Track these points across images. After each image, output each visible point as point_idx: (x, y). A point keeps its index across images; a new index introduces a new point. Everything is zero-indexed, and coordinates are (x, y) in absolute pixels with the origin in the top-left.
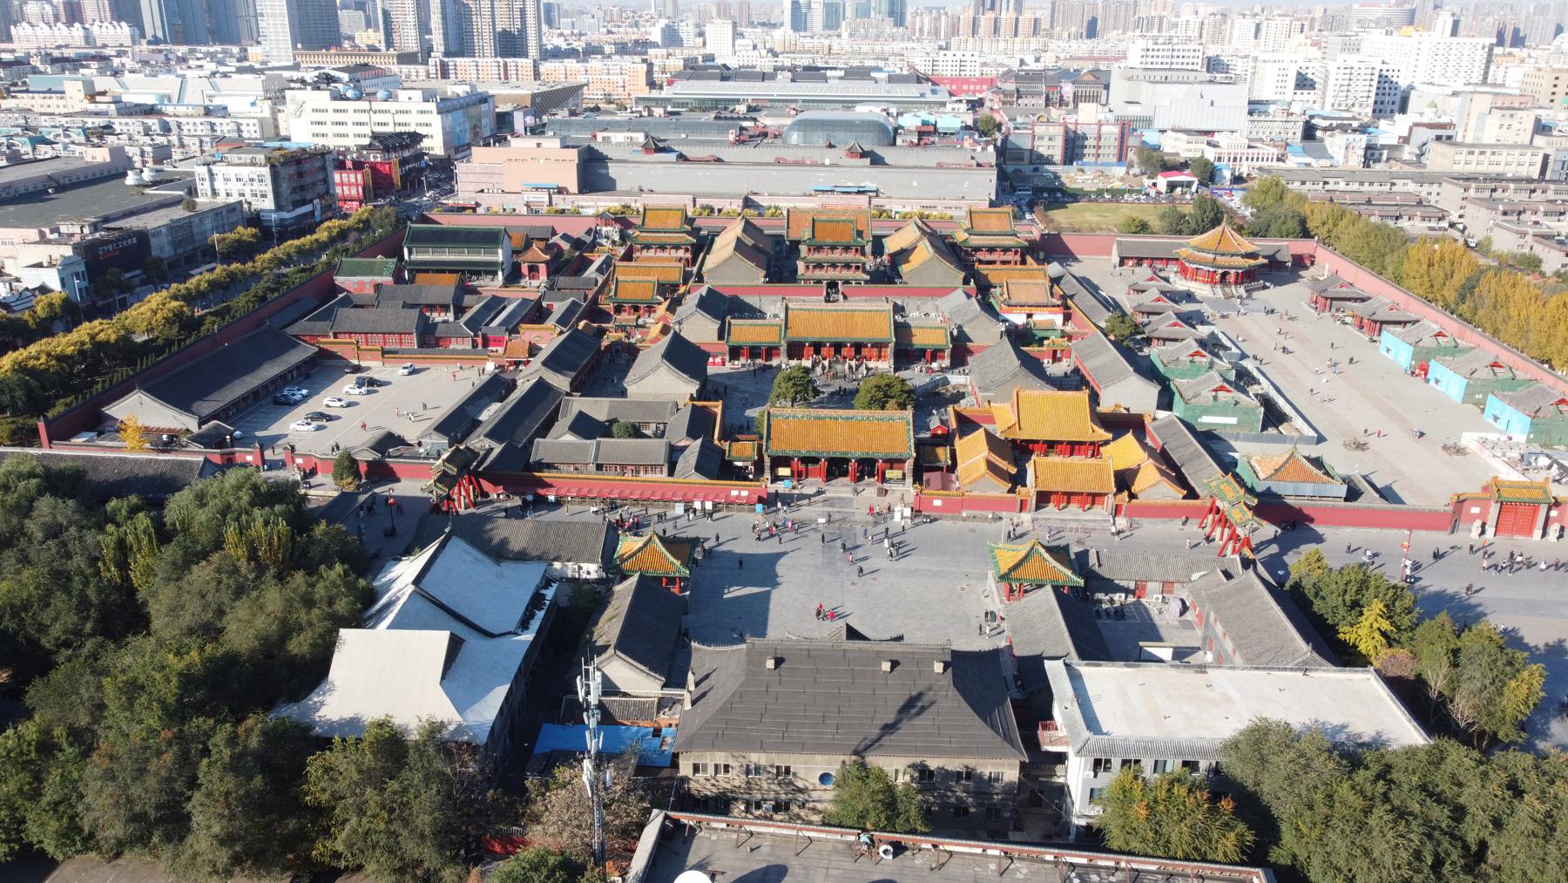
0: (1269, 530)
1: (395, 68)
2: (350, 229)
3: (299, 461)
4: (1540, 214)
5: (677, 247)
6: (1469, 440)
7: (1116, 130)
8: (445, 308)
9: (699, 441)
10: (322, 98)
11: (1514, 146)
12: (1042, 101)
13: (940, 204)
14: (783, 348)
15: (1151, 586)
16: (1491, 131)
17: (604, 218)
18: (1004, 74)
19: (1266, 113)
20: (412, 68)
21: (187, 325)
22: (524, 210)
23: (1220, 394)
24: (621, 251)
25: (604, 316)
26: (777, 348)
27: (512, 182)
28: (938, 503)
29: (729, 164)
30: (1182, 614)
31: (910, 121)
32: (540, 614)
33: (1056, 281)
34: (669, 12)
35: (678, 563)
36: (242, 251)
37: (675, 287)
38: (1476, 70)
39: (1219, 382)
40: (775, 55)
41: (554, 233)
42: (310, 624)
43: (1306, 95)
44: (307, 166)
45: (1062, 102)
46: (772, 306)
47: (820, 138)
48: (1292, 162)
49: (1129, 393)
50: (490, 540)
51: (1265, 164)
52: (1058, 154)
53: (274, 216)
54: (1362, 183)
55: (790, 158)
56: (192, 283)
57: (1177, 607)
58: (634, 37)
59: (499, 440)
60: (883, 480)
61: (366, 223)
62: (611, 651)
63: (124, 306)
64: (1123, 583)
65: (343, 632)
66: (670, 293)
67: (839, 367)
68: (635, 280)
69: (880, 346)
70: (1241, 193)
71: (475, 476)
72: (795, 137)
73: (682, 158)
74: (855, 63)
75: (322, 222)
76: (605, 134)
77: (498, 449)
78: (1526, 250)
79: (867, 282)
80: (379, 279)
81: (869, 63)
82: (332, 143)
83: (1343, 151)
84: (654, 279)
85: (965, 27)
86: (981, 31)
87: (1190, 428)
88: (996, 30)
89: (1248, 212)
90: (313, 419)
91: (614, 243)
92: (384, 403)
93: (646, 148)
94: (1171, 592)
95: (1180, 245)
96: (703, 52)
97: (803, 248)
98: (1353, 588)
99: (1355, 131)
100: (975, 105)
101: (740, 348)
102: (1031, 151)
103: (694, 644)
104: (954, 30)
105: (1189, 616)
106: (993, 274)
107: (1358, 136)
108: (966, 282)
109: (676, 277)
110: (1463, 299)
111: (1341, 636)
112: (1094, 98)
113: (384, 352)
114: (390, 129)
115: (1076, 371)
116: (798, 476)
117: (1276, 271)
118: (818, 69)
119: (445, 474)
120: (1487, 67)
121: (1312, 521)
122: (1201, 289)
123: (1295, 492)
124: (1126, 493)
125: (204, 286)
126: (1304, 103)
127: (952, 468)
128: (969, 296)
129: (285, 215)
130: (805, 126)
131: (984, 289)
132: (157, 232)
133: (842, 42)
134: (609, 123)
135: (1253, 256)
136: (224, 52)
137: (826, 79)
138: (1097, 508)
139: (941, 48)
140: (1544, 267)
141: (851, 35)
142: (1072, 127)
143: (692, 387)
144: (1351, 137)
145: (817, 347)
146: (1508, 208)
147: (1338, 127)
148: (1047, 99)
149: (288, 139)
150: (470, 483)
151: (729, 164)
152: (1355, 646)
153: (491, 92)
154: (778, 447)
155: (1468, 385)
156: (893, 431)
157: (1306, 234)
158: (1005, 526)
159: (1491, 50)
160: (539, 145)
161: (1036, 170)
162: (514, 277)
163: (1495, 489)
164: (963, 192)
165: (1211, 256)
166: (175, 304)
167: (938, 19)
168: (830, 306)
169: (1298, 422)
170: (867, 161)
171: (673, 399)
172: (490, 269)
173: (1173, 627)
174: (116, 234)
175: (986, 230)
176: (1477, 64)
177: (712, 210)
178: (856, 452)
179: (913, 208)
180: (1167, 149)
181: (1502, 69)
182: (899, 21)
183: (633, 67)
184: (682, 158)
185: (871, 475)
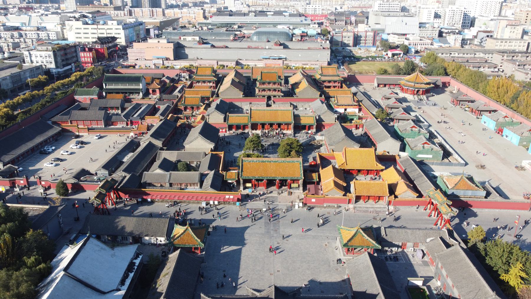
1: (113, 12)
2: (84, 76)
3: (43, 183)
5: (210, 82)
7: (372, 34)
8: (117, 108)
9: (213, 172)
10: (79, 24)
11: (516, 39)
12: (344, 23)
13: (309, 63)
14: (250, 125)
15: (409, 244)
16: (507, 33)
17: (183, 70)
18: (330, 13)
20: (119, 12)
22: (153, 67)
23: (426, 145)
24: (189, 83)
25: (179, 111)
26: (247, 125)
27: (149, 56)
28: (313, 200)
29: (230, 48)
30: (423, 258)
31: (298, 32)
32: (131, 275)
33: (355, 94)
35: (199, 241)
36: (40, 85)
37: (208, 99)
38: (497, 11)
39: (425, 140)
40: (249, 6)
41: (164, 76)
43: (437, 20)
44: (68, 51)
45: (351, 23)
46: (245, 106)
47: (264, 38)
48: (436, 45)
49: (388, 146)
50: (117, 227)
51: (426, 46)
52: (351, 43)
53: (54, 71)
54: (464, 54)
55: (253, 46)
56: (15, 100)
59: (129, 173)
60: (290, 188)
61: (91, 73)
64: (397, 243)
66: (206, 101)
67: (272, 133)
68: (192, 96)
69: (288, 124)
70: (419, 57)
71: (116, 191)
72: (255, 38)
73: (213, 46)
74: (277, 9)
76: (184, 37)
77: (128, 176)
79: (282, 96)
80: (92, 97)
81: (282, 9)
82: (83, 41)
83: (454, 41)
84: (200, 96)
89: (422, 65)
90: (54, 161)
91: (186, 79)
92: (86, 153)
93: (199, 43)
94: (418, 247)
95: (401, 79)
96: (224, 5)
97: (258, 83)
98: (506, 255)
99: (457, 33)
100: (320, 24)
101: (232, 125)
102: (342, 42)
103: (202, 295)
105: (426, 258)
106: (331, 92)
107: (459, 36)
108: (321, 96)
109: (209, 94)
110: (513, 102)
111: (501, 278)
112: (362, 22)
113: (89, 129)
114: (105, 35)
115: (366, 133)
116: (255, 186)
117: (437, 89)
118: (264, 12)
119: (100, 193)
121: (471, 206)
122: (409, 97)
123: (464, 194)
124: (393, 196)
125: (20, 101)
126: (438, 24)
127: (319, 183)
128: (322, 103)
129: (60, 70)
130: (259, 34)
131: (328, 98)
134: (186, 33)
135: (428, 84)
137: (267, 15)
138: (381, 202)
139: (307, 4)
142: (356, 33)
143: (212, 146)
144: (457, 36)
145: (263, 125)
146: (520, 63)
147: (451, 32)
148: (346, 22)
150: (114, 193)
151: (230, 48)
152: (508, 282)
153: (144, 21)
154: (246, 175)
156: (294, 167)
157: (447, 74)
159: (502, 4)
160: (159, 42)
161: (343, 49)
162: (146, 94)
164: (317, 59)
165: (413, 84)
166: (5, 110)
169: (455, 156)
170: (282, 47)
171: (204, 151)
172: (137, 91)
173: (420, 265)
176: (497, 9)
177: (224, 66)
178: (279, 177)
179: (299, 65)
180: (391, 41)
183: (198, 11)
184: (213, 46)
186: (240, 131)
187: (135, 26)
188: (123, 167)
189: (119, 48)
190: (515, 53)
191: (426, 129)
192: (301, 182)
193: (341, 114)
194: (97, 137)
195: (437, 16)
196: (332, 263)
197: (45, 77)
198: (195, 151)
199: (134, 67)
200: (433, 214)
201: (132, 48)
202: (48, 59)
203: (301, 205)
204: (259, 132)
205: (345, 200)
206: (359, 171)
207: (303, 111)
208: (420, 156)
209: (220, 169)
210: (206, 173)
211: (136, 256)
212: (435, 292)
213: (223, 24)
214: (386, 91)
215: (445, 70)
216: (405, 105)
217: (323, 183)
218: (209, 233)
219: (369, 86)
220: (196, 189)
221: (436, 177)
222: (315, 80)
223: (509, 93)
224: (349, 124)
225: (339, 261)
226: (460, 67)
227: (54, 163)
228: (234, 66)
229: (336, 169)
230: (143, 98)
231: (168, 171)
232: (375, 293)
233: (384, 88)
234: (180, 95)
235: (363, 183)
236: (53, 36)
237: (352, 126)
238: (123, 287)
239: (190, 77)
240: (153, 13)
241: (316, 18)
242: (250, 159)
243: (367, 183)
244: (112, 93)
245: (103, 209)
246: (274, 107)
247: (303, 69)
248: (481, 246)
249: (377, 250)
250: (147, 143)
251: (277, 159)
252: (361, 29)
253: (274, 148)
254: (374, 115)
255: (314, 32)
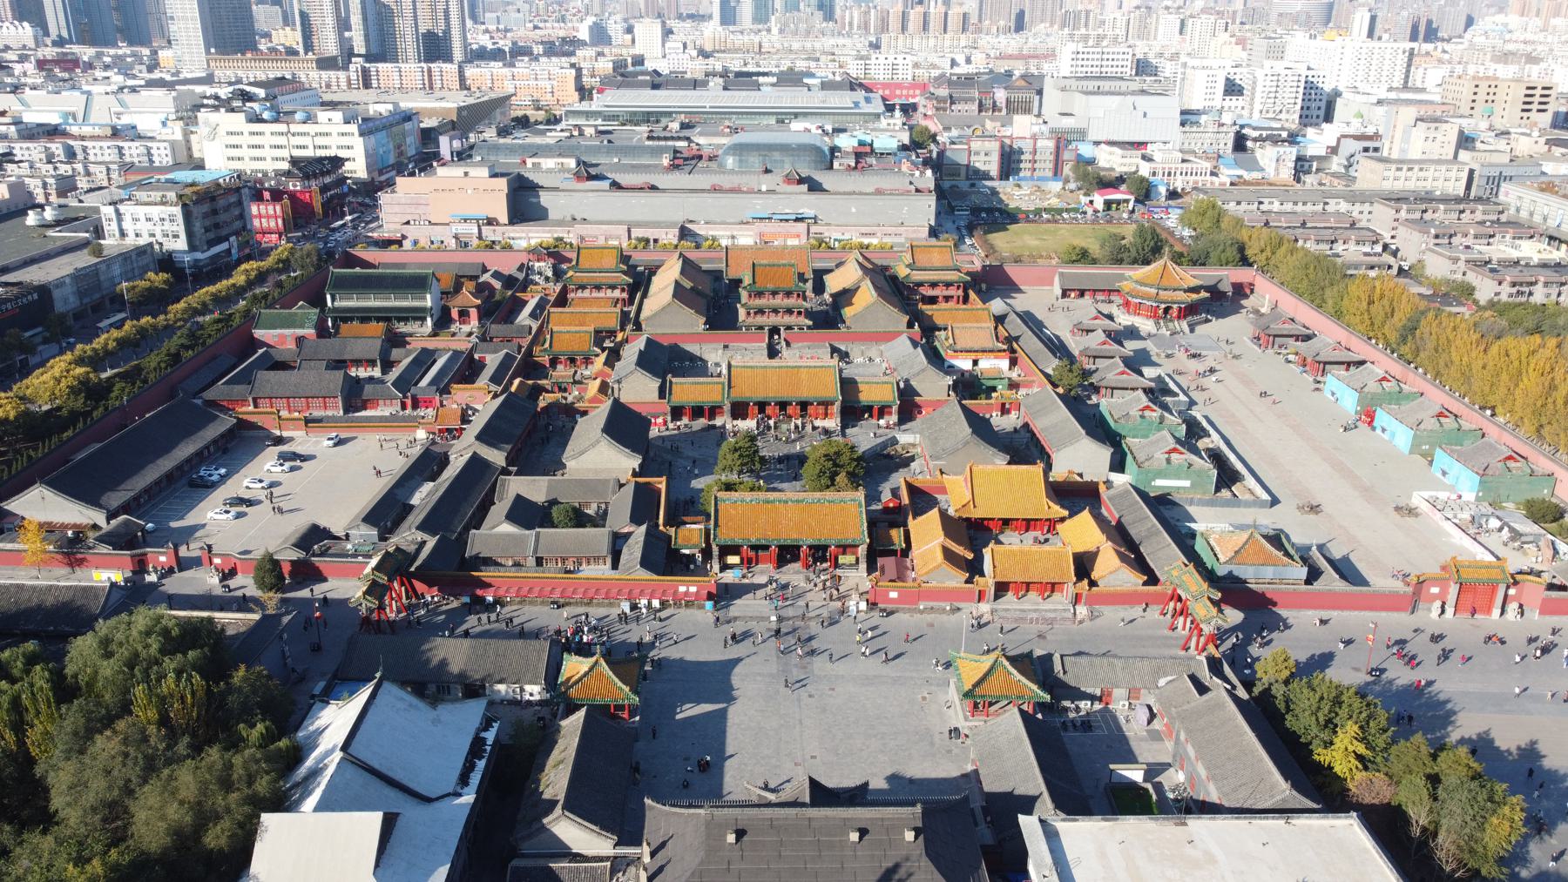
0: (1234, 616)
3: (217, 561)
4: (1470, 237)
5: (613, 287)
6: (1418, 500)
7: (1051, 144)
8: (372, 363)
9: (643, 528)
10: (237, 121)
11: (1439, 162)
12: (975, 107)
14: (727, 407)
17: (537, 252)
18: (936, 79)
19: (1197, 123)
20: (332, 74)
21: (93, 392)
22: (452, 243)
23: (1174, 456)
27: (442, 212)
28: (893, 595)
29: (664, 190)
31: (846, 142)
32: (481, 764)
33: (1000, 320)
34: (597, 10)
35: (627, 689)
36: (155, 301)
37: (612, 333)
39: (1172, 444)
41: (485, 270)
42: (228, 810)
43: (1234, 102)
45: (995, 108)
46: (713, 354)
47: (755, 161)
49: (1080, 457)
50: (428, 661)
52: (993, 168)
54: (1295, 203)
55: (727, 186)
56: (98, 343)
57: (1144, 715)
58: (562, 34)
60: (837, 565)
62: (558, 810)
63: (26, 371)
65: (266, 818)
66: (607, 343)
67: (784, 427)
69: (826, 404)
70: (1179, 211)
72: (730, 162)
73: (616, 186)
75: (239, 262)
76: (535, 160)
78: (1459, 277)
80: (300, 332)
81: (801, 65)
82: (248, 166)
85: (894, 23)
86: (911, 26)
87: (1143, 495)
88: (925, 27)
90: (231, 505)
91: (547, 279)
92: (310, 486)
95: (1122, 278)
97: (744, 294)
103: (648, 801)
104: (884, 26)
105: (1157, 725)
108: (910, 325)
109: (613, 322)
110: (1404, 340)
111: (1316, 757)
112: (1027, 110)
114: (309, 153)
115: (1026, 425)
116: (748, 563)
119: (374, 584)
120: (1408, 71)
121: (1275, 604)
122: (1145, 325)
123: (1258, 576)
124: (1086, 581)
125: (112, 345)
128: (915, 344)
129: (199, 255)
130: (739, 149)
132: (60, 283)
133: (772, 38)
134: (539, 147)
136: (134, 55)
137: (758, 87)
138: (1057, 596)
140: (1477, 295)
141: (781, 31)
142: (1008, 141)
143: (634, 462)
145: (762, 406)
146: (1440, 231)
148: (981, 105)
149: (200, 166)
150: (402, 584)
151: (664, 190)
152: (1330, 768)
154: (726, 535)
155: (1415, 436)
156: (843, 513)
157: (1245, 261)
158: (965, 618)
160: (466, 174)
161: (973, 185)
162: (443, 321)
163: (1454, 569)
165: (1154, 291)
166: (80, 370)
167: (867, 13)
168: (775, 362)
169: (1250, 481)
172: (418, 315)
173: (1142, 739)
174: (15, 290)
175: (928, 265)
176: (1398, 68)
177: (647, 241)
178: (807, 540)
180: (1102, 163)
181: (1421, 71)
182: (829, 16)
184: (616, 186)
185: (824, 560)
186: (702, 422)
187: (391, 125)
188: (416, 518)
189: (350, 189)
190: (1431, 200)
191: (1180, 412)
192: (862, 550)
193: (963, 373)
194: (331, 443)
195: (1232, 89)
196: (937, 738)
197: (164, 276)
198: (591, 476)
199: (399, 243)
200: (1180, 626)
201: (393, 192)
202: (167, 226)
203: (863, 606)
204: (749, 424)
205: (971, 592)
206: (1006, 522)
207: (863, 365)
208: (1159, 482)
209: (661, 521)
210: (626, 530)
211: (486, 725)
212: (1171, 796)
213: (635, 113)
214: (1085, 308)
215: (1242, 249)
216: (1131, 346)
217: (915, 552)
218: (645, 676)
219: (1039, 297)
220: (603, 570)
221: (1193, 535)
222: (894, 279)
223: (1396, 318)
224: (984, 402)
225: (955, 732)
226: (1280, 244)
227: (234, 510)
228: (675, 242)
229: (951, 518)
230: (434, 334)
231: (529, 527)
232: (1032, 792)
233: (1081, 301)
234: (535, 326)
235: (1012, 552)
236: (162, 156)
237: (990, 408)
238: (466, 790)
239: (558, 274)
240: (430, 76)
241: (898, 92)
242: (734, 495)
243: (1022, 552)
244: (352, 319)
245: (379, 621)
246: (789, 356)
247: (863, 247)
248: (1278, 691)
249: (1041, 706)
250: (467, 457)
251: (802, 495)
252: (1021, 128)
253: (792, 466)
254: (1047, 376)
255: (892, 144)
